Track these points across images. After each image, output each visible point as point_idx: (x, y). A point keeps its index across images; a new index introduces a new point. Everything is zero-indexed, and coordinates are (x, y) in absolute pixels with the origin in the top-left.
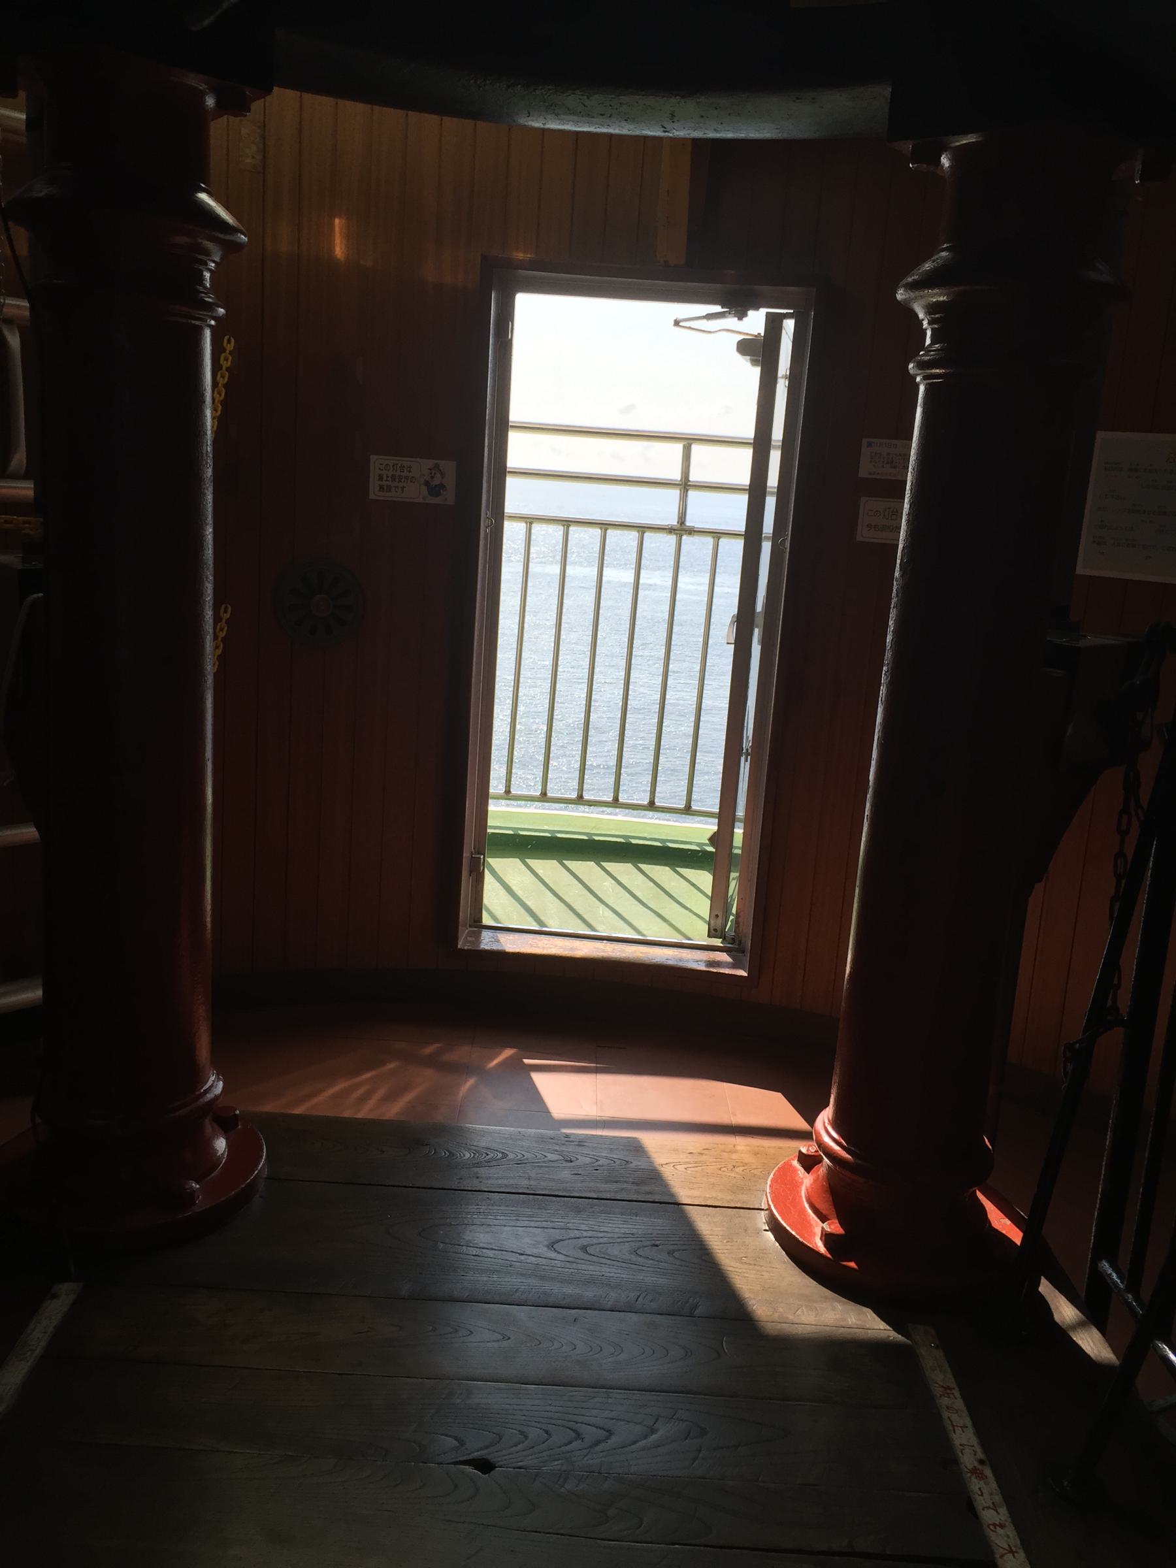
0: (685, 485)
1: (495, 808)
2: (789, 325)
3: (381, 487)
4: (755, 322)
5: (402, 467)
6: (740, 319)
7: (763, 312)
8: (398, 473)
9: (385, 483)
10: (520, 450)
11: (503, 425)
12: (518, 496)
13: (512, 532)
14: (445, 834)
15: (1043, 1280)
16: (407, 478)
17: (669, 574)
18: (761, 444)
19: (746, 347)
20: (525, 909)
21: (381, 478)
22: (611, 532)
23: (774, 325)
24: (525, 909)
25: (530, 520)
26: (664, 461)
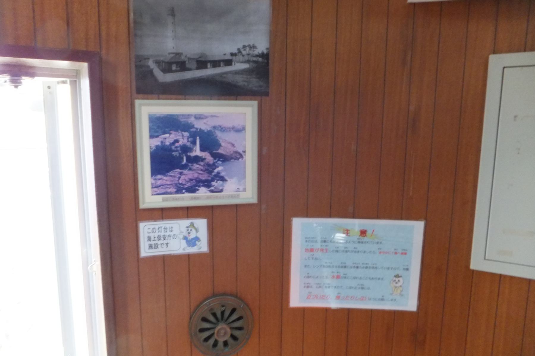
5: (165, 229)
9: (152, 243)
16: (169, 236)
21: (149, 239)
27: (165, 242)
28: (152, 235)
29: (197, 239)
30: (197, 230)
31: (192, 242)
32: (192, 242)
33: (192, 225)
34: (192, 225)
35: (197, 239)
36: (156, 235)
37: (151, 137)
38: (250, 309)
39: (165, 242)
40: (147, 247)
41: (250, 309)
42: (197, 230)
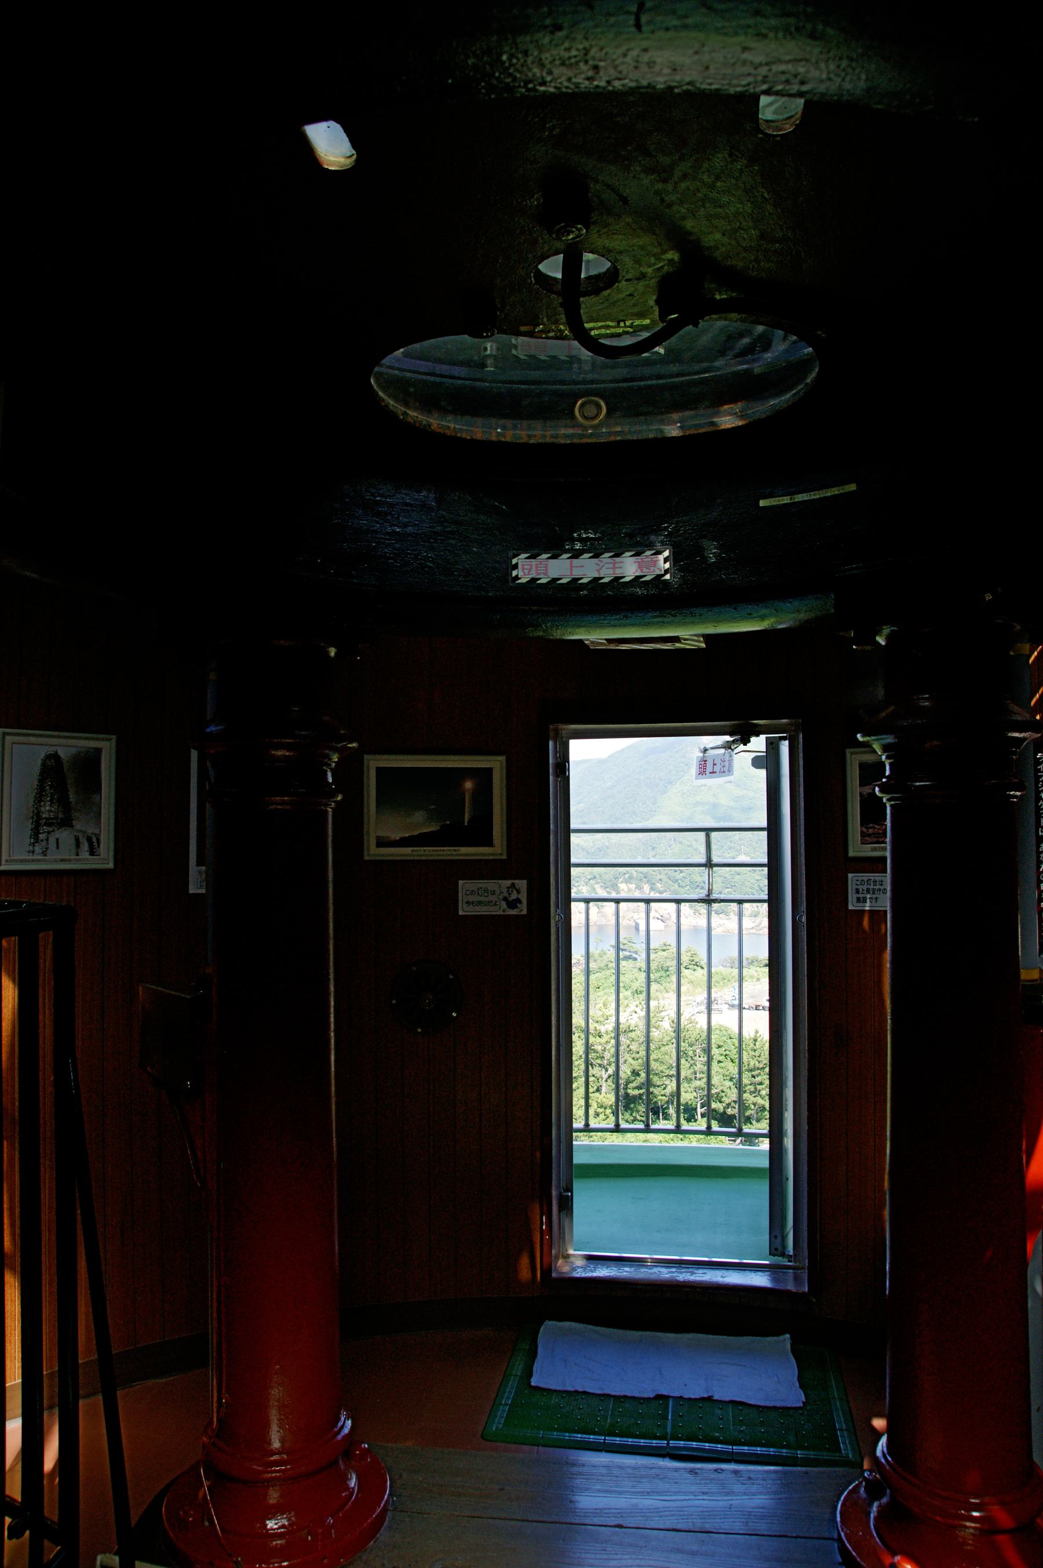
0: (709, 864)
1: (580, 1141)
2: (785, 747)
3: (858, 900)
4: (758, 743)
5: (875, 881)
6: (745, 744)
7: (763, 738)
8: (872, 887)
9: (861, 896)
10: (580, 847)
11: (566, 831)
12: (581, 883)
13: (577, 910)
14: (535, 1168)
15: (19, 1499)
16: (879, 890)
17: (651, 928)
18: (773, 828)
19: (756, 763)
20: (603, 1234)
21: (857, 891)
22: (622, 905)
23: (772, 747)
24: (603, 1234)
25: (587, 901)
26: (693, 848)
27: (874, 896)
28: (860, 887)
29: (518, 901)
30: (518, 892)
31: (513, 904)
32: (513, 904)
33: (513, 885)
34: (513, 885)
35: (518, 901)
36: (865, 887)
37: (861, 785)
38: (693, 1553)
39: (874, 896)
40: (855, 900)
41: (693, 1553)
42: (518, 892)
